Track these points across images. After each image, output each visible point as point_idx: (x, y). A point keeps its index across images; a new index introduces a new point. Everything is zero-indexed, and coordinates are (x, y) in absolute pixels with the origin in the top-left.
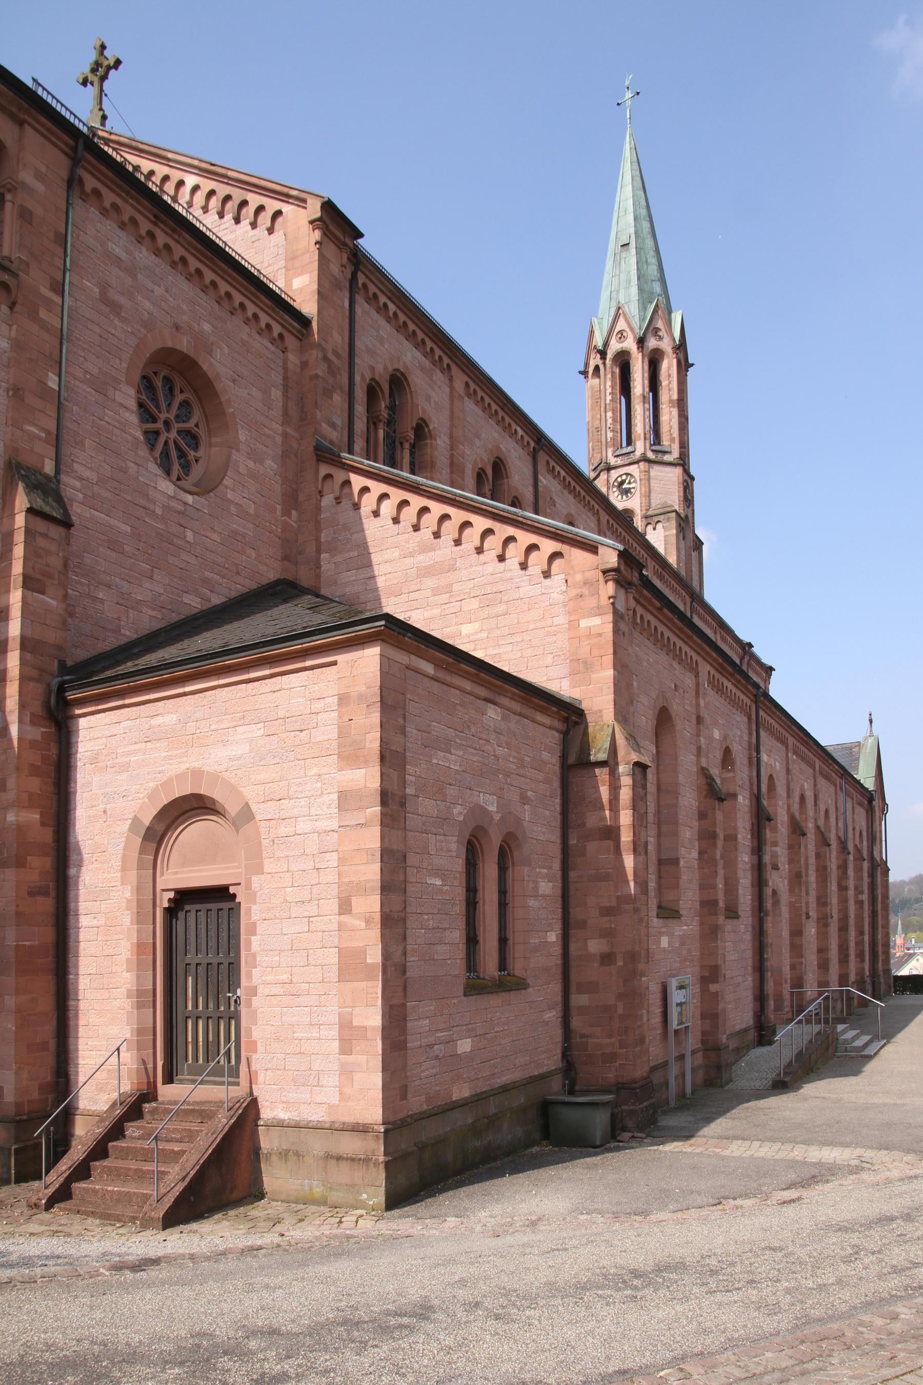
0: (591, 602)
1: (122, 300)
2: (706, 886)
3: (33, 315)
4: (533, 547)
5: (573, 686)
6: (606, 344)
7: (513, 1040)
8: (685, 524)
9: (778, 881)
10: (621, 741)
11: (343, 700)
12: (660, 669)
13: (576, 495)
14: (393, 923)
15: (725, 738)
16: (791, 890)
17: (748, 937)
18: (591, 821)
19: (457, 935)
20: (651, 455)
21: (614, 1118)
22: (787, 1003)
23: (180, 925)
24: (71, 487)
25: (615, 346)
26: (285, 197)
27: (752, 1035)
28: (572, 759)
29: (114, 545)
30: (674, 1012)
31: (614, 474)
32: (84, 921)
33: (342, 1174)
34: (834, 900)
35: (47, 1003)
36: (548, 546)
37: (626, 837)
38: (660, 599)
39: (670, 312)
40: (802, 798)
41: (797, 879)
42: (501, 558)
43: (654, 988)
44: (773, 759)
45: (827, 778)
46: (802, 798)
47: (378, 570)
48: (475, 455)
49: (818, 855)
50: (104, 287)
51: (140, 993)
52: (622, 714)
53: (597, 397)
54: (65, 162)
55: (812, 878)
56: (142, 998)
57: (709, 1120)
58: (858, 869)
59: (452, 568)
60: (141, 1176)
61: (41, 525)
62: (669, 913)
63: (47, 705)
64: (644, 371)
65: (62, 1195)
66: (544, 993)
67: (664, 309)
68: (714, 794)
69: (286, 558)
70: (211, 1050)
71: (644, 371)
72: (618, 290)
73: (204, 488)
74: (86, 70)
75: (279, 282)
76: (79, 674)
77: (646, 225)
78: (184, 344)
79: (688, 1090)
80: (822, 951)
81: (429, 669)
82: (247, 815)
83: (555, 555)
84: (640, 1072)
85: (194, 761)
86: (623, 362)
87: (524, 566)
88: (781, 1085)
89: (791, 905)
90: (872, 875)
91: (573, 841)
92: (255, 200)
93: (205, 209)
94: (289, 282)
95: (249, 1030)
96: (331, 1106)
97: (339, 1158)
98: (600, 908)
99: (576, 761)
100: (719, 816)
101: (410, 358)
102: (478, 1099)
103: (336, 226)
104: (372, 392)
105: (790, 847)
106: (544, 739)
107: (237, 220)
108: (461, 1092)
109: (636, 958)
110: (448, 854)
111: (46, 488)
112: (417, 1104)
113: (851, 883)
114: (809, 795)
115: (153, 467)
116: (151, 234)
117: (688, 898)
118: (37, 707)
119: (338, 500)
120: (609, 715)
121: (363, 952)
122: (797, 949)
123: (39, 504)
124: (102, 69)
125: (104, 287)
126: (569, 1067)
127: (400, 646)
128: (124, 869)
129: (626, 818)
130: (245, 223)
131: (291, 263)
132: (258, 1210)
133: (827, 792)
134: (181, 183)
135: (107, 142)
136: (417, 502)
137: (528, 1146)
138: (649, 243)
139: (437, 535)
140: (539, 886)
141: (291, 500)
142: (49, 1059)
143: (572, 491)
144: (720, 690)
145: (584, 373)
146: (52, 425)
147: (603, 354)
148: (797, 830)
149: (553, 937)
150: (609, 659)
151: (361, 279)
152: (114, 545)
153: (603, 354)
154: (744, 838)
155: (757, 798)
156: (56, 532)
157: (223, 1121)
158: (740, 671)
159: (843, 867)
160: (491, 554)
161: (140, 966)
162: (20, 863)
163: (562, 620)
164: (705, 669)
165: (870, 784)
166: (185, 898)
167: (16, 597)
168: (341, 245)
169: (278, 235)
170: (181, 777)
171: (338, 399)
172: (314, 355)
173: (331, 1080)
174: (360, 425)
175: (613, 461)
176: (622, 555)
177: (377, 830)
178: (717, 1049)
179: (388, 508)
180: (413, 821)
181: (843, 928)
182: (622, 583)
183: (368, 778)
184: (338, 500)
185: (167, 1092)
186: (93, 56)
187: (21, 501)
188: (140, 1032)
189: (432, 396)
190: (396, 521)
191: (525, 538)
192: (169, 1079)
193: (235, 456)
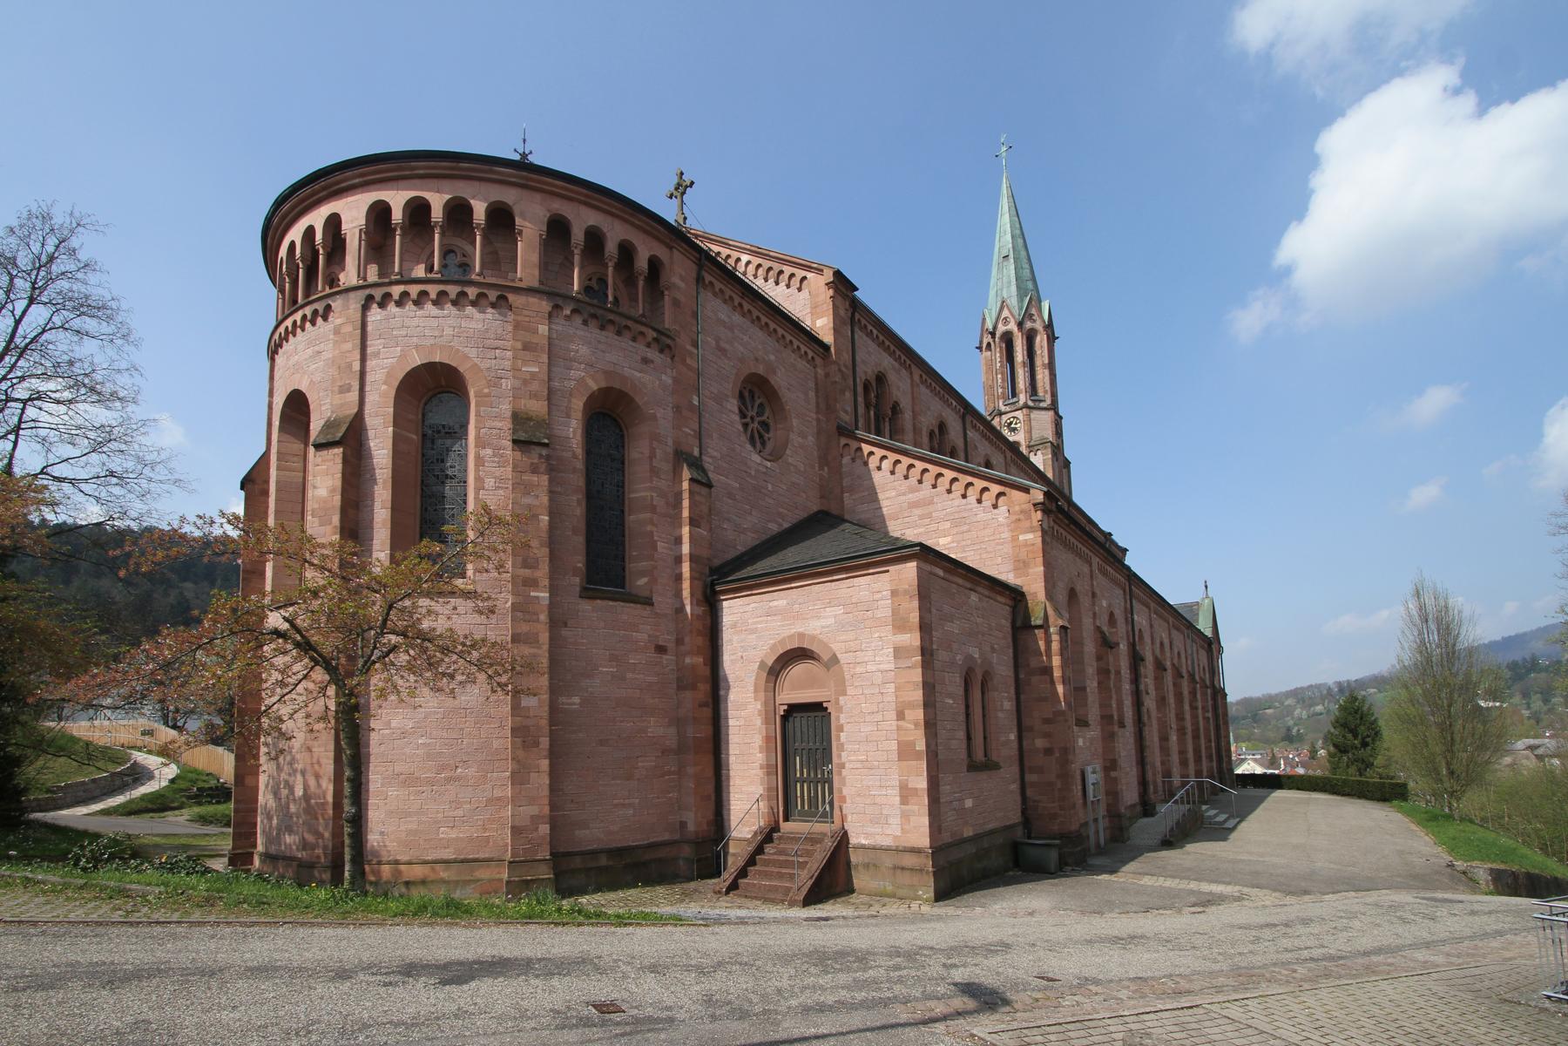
0: (1027, 524)
1: (727, 346)
2: (1104, 705)
3: (684, 362)
4: (985, 489)
5: (1016, 577)
6: (995, 328)
7: (993, 803)
8: (1057, 449)
9: (1150, 702)
10: (1050, 611)
11: (894, 593)
12: (1072, 565)
13: (991, 442)
14: (930, 726)
15: (1110, 605)
16: (1158, 708)
17: (1132, 740)
18: (1034, 663)
19: (961, 734)
20: (1030, 403)
21: (1061, 857)
22: (1160, 788)
23: (790, 726)
24: (708, 463)
25: (1001, 328)
26: (808, 268)
27: (1139, 808)
28: (1019, 624)
29: (730, 496)
30: (1090, 789)
31: (1004, 418)
32: (731, 722)
33: (905, 878)
34: (1188, 716)
35: (710, 772)
36: (995, 489)
37: (1057, 673)
38: (1065, 522)
39: (1040, 302)
40: (1162, 644)
41: (1161, 701)
42: (964, 496)
43: (1078, 772)
44: (1141, 619)
45: (1178, 629)
46: (1162, 644)
47: (884, 503)
48: (927, 422)
49: (1175, 685)
50: (718, 340)
51: (768, 766)
52: (1050, 595)
53: (990, 363)
54: (695, 267)
55: (1172, 701)
56: (769, 769)
57: (1124, 863)
58: (1204, 694)
59: (931, 503)
60: (781, 876)
61: (697, 488)
62: (1083, 723)
63: (705, 594)
64: (1024, 345)
65: (733, 887)
66: (1010, 771)
67: (1036, 301)
68: (1106, 644)
69: (822, 497)
70: (813, 802)
71: (1024, 345)
72: (1002, 286)
73: (776, 456)
74: (672, 189)
75: (807, 323)
76: (724, 575)
77: (1020, 241)
78: (761, 370)
79: (1102, 841)
80: (1182, 752)
81: (941, 573)
82: (835, 660)
83: (1000, 494)
84: (1074, 827)
85: (799, 628)
86: (1008, 339)
87: (979, 501)
88: (1167, 844)
89: (1159, 719)
90: (1214, 698)
91: (1022, 676)
92: (788, 270)
93: (755, 276)
94: (814, 322)
95: (840, 791)
96: (895, 837)
97: (903, 869)
98: (1354, 699)
99: (1021, 623)
100: (1111, 659)
101: (886, 362)
102: (976, 838)
103: (842, 286)
104: (866, 387)
105: (1156, 678)
106: (1001, 612)
107: (777, 283)
108: (968, 832)
109: (1066, 752)
110: (954, 683)
111: (696, 464)
112: (946, 838)
113: (1200, 705)
114: (1166, 642)
115: (749, 447)
116: (741, 305)
117: (1094, 713)
118: (699, 595)
119: (853, 460)
120: (1042, 596)
121: (913, 743)
122: (1165, 750)
123: (696, 476)
124: (682, 188)
125: (718, 340)
126: (1027, 821)
127: (926, 561)
128: (756, 691)
129: (1056, 661)
130: (782, 285)
131: (815, 311)
132: (854, 898)
133: (1178, 638)
134: (738, 260)
135: (697, 236)
136: (906, 461)
137: (1007, 870)
138: (1023, 253)
139: (920, 482)
140: (1004, 704)
141: (824, 460)
142: (712, 805)
143: (988, 439)
144: (1105, 574)
145: (980, 348)
146: (696, 427)
147: (993, 334)
148: (1160, 666)
149: (1013, 737)
150: (1040, 560)
151: (857, 316)
152: (730, 496)
153: (993, 334)
154: (1126, 673)
155: (1132, 646)
156: (704, 490)
157: (829, 844)
158: (1108, 552)
159: (1193, 693)
160: (957, 493)
161: (768, 750)
162: (694, 687)
163: (1006, 535)
164: (1096, 560)
165: (1208, 633)
166: (793, 709)
167: (686, 530)
168: (845, 296)
169: (805, 292)
170: (792, 636)
171: (848, 395)
172: (834, 368)
173: (895, 821)
174: (861, 410)
175: (1003, 408)
176: (1046, 494)
177: (919, 670)
178: (1119, 816)
179: (886, 465)
180: (937, 664)
181: (1196, 737)
182: (1046, 511)
183: (913, 639)
184: (853, 460)
185: (786, 827)
186: (675, 180)
187: (686, 474)
188: (769, 789)
189: (901, 386)
190: (893, 473)
191: (980, 484)
192: (786, 819)
193: (792, 436)
